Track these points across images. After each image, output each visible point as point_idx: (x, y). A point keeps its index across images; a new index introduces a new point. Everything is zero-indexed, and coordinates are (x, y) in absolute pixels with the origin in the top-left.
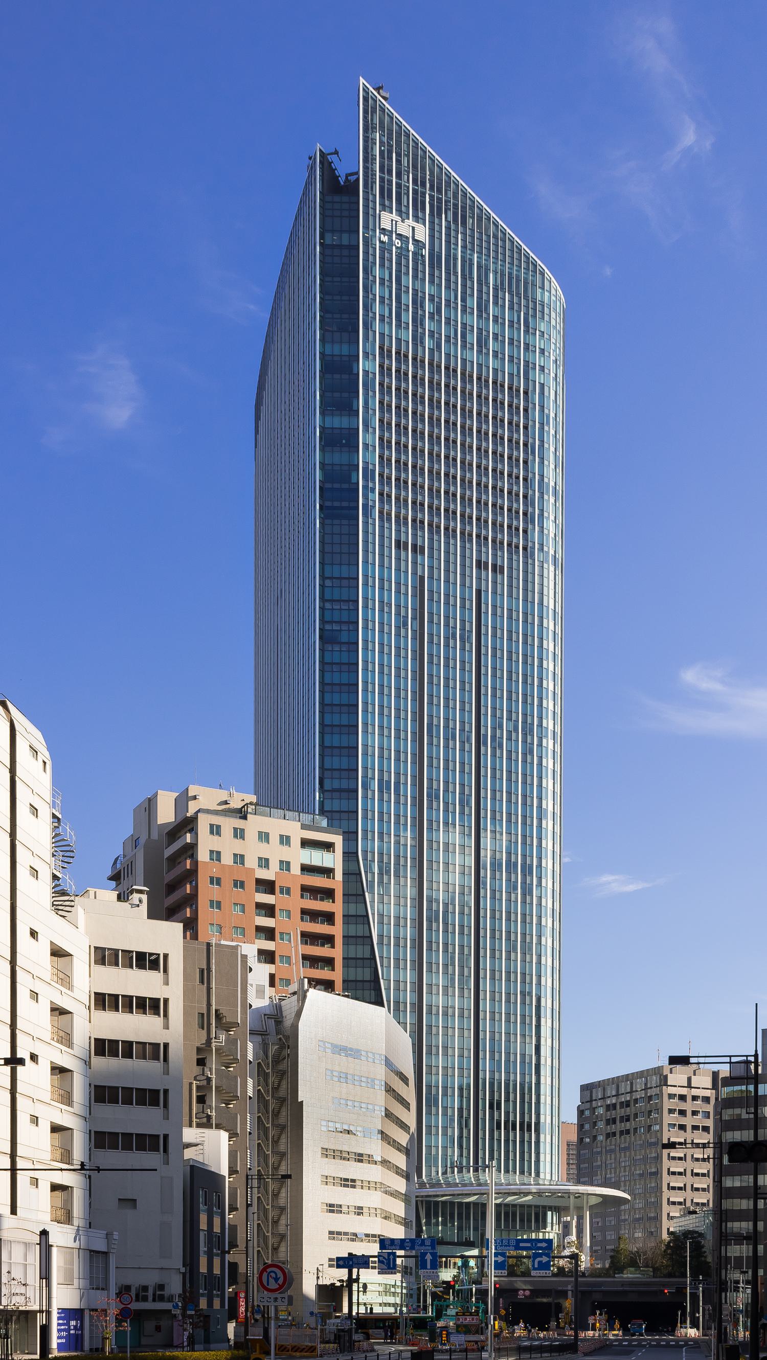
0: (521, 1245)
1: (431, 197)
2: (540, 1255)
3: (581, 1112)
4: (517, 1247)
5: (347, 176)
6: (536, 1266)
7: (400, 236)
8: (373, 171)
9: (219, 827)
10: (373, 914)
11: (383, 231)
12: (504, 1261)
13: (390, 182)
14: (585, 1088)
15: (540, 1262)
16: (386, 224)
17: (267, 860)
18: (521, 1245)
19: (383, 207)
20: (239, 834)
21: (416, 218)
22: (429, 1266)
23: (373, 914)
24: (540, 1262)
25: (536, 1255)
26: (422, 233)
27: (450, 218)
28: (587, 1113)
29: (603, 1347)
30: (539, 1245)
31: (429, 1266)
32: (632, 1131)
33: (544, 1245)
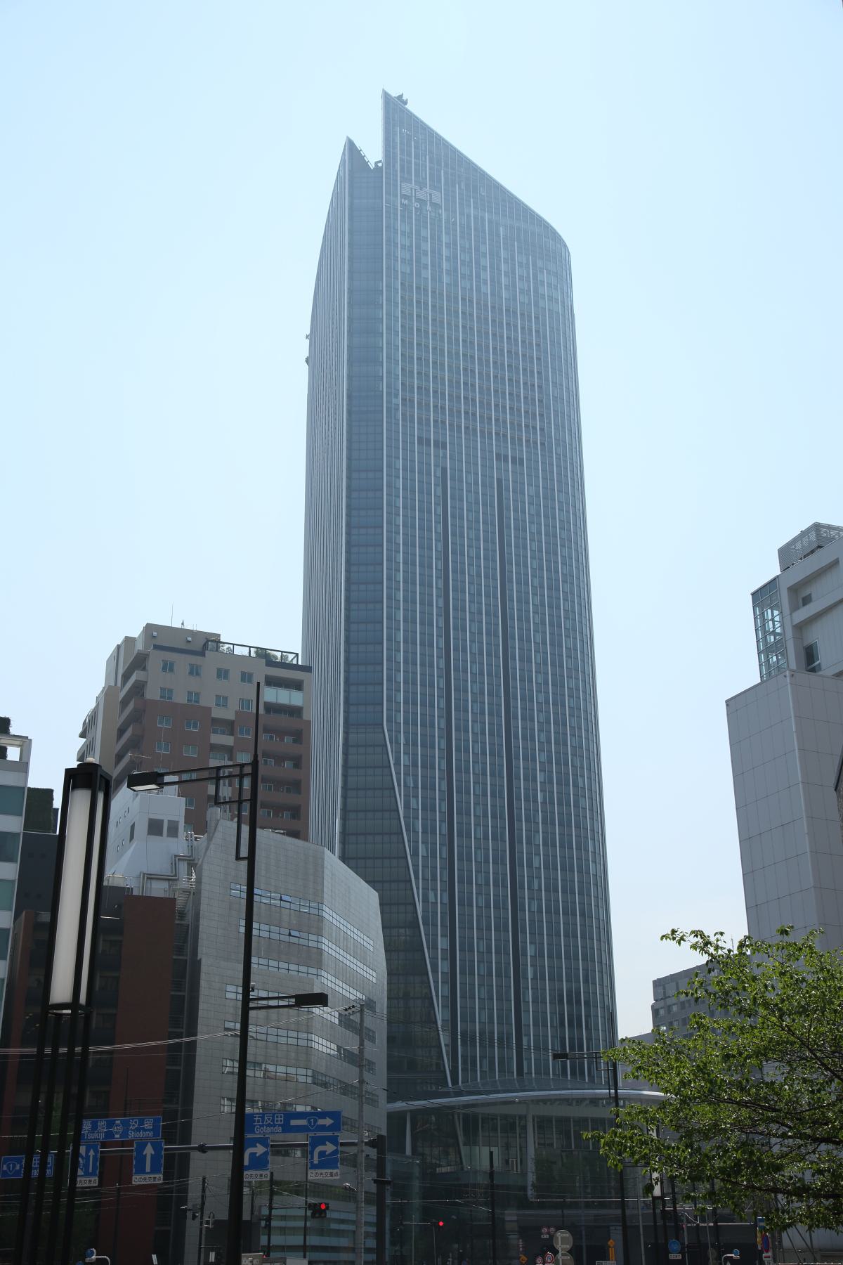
0: (294, 1123)
1: (446, 173)
2: (322, 1141)
3: (655, 1012)
4: (287, 1128)
5: (376, 163)
6: (316, 1161)
7: (418, 200)
8: (395, 154)
9: (172, 665)
10: (399, 785)
11: (404, 196)
12: (335, 1152)
13: (410, 162)
14: (657, 983)
15: (322, 1154)
16: (407, 192)
17: (226, 698)
18: (294, 1123)
19: (403, 179)
20: (195, 671)
21: (433, 187)
22: (148, 1169)
23: (399, 785)
24: (322, 1154)
25: (317, 1142)
26: (439, 198)
27: (463, 187)
28: (662, 1012)
29: (813, 1252)
30: (321, 1122)
31: (148, 1169)
32: (142, 829)
33: (328, 1122)
